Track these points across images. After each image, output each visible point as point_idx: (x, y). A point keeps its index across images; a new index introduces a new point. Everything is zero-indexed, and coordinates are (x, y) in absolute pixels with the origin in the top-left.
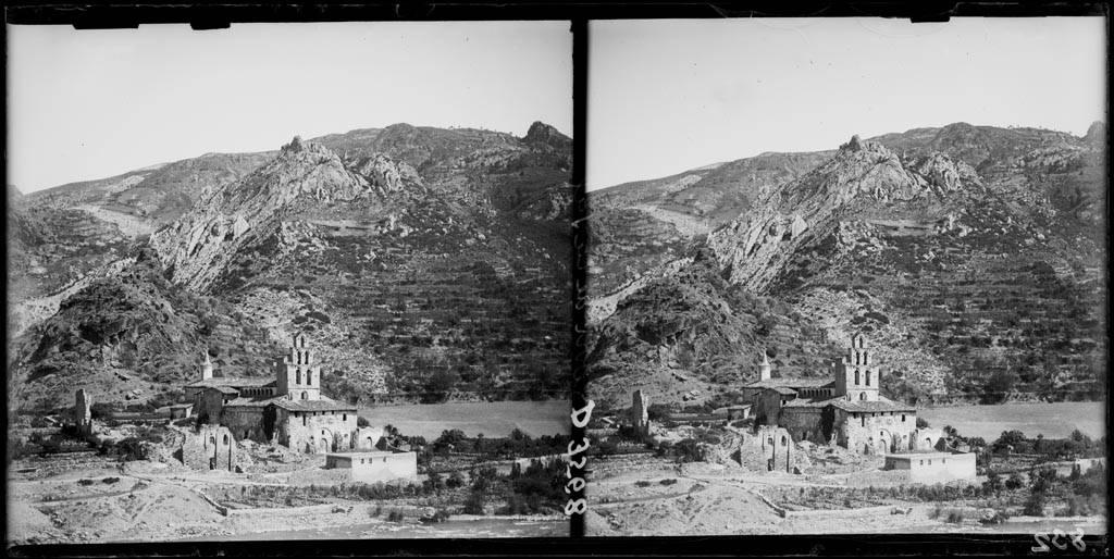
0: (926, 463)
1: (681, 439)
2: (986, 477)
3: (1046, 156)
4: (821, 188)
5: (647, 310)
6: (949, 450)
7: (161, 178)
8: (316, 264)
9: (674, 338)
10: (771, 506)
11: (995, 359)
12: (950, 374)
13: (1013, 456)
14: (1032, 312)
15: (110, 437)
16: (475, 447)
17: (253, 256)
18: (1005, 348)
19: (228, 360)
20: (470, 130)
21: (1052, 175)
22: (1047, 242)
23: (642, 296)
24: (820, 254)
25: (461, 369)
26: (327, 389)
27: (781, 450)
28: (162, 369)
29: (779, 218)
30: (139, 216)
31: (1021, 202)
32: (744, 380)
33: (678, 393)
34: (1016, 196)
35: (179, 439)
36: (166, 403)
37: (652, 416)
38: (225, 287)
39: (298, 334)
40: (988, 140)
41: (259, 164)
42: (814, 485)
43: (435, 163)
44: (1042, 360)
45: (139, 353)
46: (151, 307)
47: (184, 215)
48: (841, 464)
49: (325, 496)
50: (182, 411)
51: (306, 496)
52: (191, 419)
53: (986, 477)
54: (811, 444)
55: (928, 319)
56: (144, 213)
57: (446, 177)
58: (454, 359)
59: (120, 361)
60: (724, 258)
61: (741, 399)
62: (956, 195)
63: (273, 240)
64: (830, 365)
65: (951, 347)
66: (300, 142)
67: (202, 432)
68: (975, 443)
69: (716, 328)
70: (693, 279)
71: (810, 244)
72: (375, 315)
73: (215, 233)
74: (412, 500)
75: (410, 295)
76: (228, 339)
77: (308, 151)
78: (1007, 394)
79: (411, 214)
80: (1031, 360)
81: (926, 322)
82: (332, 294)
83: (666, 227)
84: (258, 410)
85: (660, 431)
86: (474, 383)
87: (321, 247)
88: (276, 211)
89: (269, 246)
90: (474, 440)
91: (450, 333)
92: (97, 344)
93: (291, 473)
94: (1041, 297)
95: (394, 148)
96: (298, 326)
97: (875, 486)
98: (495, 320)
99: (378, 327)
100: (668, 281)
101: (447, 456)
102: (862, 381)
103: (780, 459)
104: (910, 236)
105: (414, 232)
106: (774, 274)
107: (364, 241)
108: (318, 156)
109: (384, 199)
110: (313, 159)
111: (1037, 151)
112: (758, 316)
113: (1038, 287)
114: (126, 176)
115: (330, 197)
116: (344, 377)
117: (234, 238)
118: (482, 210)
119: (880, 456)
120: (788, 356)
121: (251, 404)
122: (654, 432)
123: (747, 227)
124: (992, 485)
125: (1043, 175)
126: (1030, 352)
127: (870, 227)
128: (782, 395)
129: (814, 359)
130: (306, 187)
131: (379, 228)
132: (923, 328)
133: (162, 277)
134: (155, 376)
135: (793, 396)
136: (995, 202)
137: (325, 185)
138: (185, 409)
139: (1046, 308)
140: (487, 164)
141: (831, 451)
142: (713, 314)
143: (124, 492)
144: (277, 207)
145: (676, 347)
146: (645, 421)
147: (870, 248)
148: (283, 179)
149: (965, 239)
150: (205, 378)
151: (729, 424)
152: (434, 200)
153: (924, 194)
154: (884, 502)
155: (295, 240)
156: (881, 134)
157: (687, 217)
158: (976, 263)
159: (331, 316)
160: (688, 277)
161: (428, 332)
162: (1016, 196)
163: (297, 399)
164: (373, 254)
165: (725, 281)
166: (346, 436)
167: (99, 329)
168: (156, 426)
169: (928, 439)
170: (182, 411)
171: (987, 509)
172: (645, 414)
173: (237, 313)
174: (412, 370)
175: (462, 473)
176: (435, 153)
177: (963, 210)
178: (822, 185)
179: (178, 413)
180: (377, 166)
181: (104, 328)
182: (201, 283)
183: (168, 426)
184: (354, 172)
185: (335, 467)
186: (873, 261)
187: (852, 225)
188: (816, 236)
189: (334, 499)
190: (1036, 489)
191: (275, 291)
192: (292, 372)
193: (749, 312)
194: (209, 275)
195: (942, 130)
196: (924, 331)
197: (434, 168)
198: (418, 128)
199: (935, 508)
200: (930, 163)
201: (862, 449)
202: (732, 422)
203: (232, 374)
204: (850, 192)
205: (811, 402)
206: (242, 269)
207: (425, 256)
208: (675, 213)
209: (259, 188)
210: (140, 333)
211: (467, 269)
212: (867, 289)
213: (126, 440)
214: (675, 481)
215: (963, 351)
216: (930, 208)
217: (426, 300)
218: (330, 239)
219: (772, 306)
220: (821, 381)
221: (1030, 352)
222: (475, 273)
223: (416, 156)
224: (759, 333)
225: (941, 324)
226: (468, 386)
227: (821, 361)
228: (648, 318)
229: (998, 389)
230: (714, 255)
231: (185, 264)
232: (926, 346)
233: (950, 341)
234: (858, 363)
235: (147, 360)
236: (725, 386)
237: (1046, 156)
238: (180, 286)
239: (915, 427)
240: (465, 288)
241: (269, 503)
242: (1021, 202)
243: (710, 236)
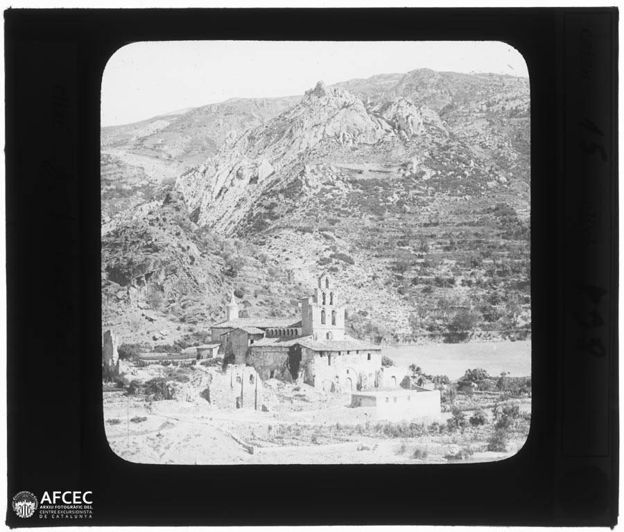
1: (151, 378)
2: (451, 413)
3: (507, 100)
4: (287, 133)
5: (117, 252)
6: (414, 388)
7: (186, 124)
8: (340, 207)
9: (143, 279)
10: (240, 443)
11: (458, 299)
12: (415, 314)
13: (476, 393)
14: (494, 253)
15: (155, 376)
16: (497, 386)
17: (278, 199)
18: (469, 289)
19: (253, 302)
20: (491, 75)
21: (514, 119)
22: (509, 184)
23: (112, 239)
24: (286, 197)
25: (484, 309)
26: (352, 330)
27: (249, 388)
28: (189, 310)
29: (246, 162)
30: (164, 160)
31: (483, 146)
32: (212, 320)
33: (148, 333)
34: (478, 140)
35: (205, 379)
36: (192, 343)
37: (123, 355)
38: (250, 229)
39: (322, 275)
40: (450, 85)
41: (282, 108)
42: (281, 422)
43: (456, 108)
44: (505, 299)
45: (166, 295)
46: (177, 249)
47: (209, 159)
48: (307, 401)
49: (350, 435)
50: (208, 351)
51: (332, 435)
52: (216, 361)
53: (451, 413)
54: (279, 382)
55: (393, 260)
56: (170, 157)
57: (467, 121)
58: (475, 298)
59: (147, 302)
60: (192, 201)
61: (209, 339)
62: (419, 139)
63: (297, 183)
64: (297, 305)
65: (416, 287)
66: (323, 87)
67: (229, 371)
68: (441, 381)
69: (184, 270)
70: (161, 221)
71: (277, 188)
72: (399, 256)
73: (239, 176)
74: (436, 438)
75: (432, 236)
76: (253, 280)
77: (331, 96)
78: (470, 333)
79: (433, 157)
80: (494, 300)
81: (391, 263)
82: (356, 236)
83: (135, 171)
84: (284, 350)
85: (131, 370)
86: (497, 322)
87: (344, 190)
88: (300, 155)
89: (293, 189)
90: (495, 379)
91: (472, 274)
92: (124, 285)
93: (317, 411)
94: (503, 238)
95: (415, 93)
96: (322, 267)
97: (342, 424)
98: (516, 261)
99: (401, 268)
100: (137, 223)
101: (470, 394)
102: (329, 320)
103: (249, 397)
104: (375, 179)
105: (437, 175)
106: (242, 216)
107: (387, 184)
108: (341, 101)
109: (406, 142)
110: (336, 104)
111: (499, 96)
112: (226, 257)
113: (500, 229)
114: (152, 121)
115: (354, 140)
116: (368, 317)
117: (259, 181)
118: (503, 152)
119: (346, 394)
120: (256, 296)
121: (277, 344)
122: (125, 371)
123: (215, 171)
124: (457, 422)
125: (505, 120)
126: (492, 292)
127: (335, 170)
128: (249, 335)
129: (281, 299)
130: (330, 132)
131: (402, 171)
132: (387, 268)
133: (188, 220)
134: (182, 317)
135: (261, 336)
136: (458, 146)
137: (348, 129)
138: (211, 350)
139: (508, 249)
140: (507, 108)
141: (297, 389)
142: (182, 256)
143: (152, 432)
144: (301, 151)
145: (145, 288)
146: (115, 360)
147: (334, 191)
148: (307, 124)
149: (428, 182)
150: (231, 319)
151: (198, 363)
152: (456, 143)
153: (388, 138)
154: (349, 438)
155: (319, 183)
156: (346, 80)
157: (155, 161)
158: (440, 205)
159: (355, 257)
160: (157, 219)
161: (451, 273)
162: (478, 140)
163: (322, 339)
164: (396, 196)
165: (193, 224)
166: (370, 375)
167: (126, 271)
168: (184, 366)
169: (393, 377)
170: (208, 351)
171: (452, 445)
172: (116, 354)
173: (262, 255)
174: (435, 310)
175: (485, 411)
176: (457, 98)
177: (427, 154)
178: (289, 130)
179: (205, 354)
180: (400, 111)
181: (131, 270)
182: (226, 225)
183: (195, 367)
184: (377, 116)
185: (359, 405)
186: (339, 203)
187: (318, 168)
188: (283, 180)
189: (359, 437)
190: (500, 425)
191: (300, 233)
192: (316, 313)
193: (216, 254)
194: (235, 218)
195: (405, 76)
196: (389, 272)
197: (455, 112)
198: (440, 73)
199: (401, 444)
200: (394, 107)
201: (329, 387)
202: (201, 361)
203: (258, 314)
204: (315, 136)
205: (279, 341)
206: (267, 211)
207: (447, 199)
208: (144, 158)
209: (283, 132)
211: (489, 211)
212: (332, 231)
213: (155, 380)
214: (145, 419)
215: (427, 291)
216: (394, 151)
217: (449, 242)
218: (354, 182)
219: (239, 248)
220: (288, 321)
221: (492, 292)
222: (497, 215)
223: (438, 100)
224: (227, 274)
225: (406, 265)
226: (489, 326)
227: (288, 302)
228: (118, 259)
229: (462, 328)
230: (182, 199)
231: (210, 207)
232: (391, 286)
233: (415, 281)
234: (324, 303)
235: (174, 301)
236: (194, 326)
237: (507, 100)
238: (206, 228)
239: (381, 366)
240: (487, 229)
241: (295, 442)
242: (483, 146)
243: (178, 181)
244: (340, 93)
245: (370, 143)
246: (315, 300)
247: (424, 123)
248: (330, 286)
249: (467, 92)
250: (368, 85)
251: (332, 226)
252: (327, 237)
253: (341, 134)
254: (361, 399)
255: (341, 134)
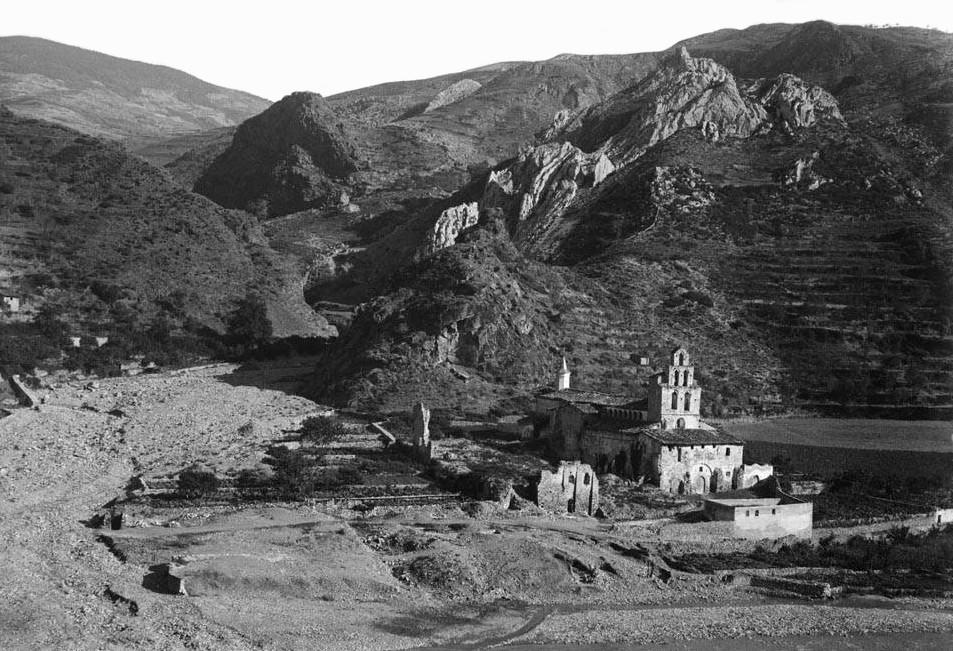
0: (752, 515)
102: (681, 404)
115: (720, 132)
139: (924, 362)
147: (693, 203)
149: (815, 193)
184: (752, 100)
197: (858, 88)
210: (482, 324)
234: (676, 384)
239: (741, 463)
244: (706, 66)
245: (741, 137)
246: (666, 380)
247: (815, 110)
248: (686, 363)
249: (876, 56)
250: (742, 40)
251: (686, 252)
252: (678, 268)
253: (705, 124)
254: (715, 510)
255: (705, 124)
